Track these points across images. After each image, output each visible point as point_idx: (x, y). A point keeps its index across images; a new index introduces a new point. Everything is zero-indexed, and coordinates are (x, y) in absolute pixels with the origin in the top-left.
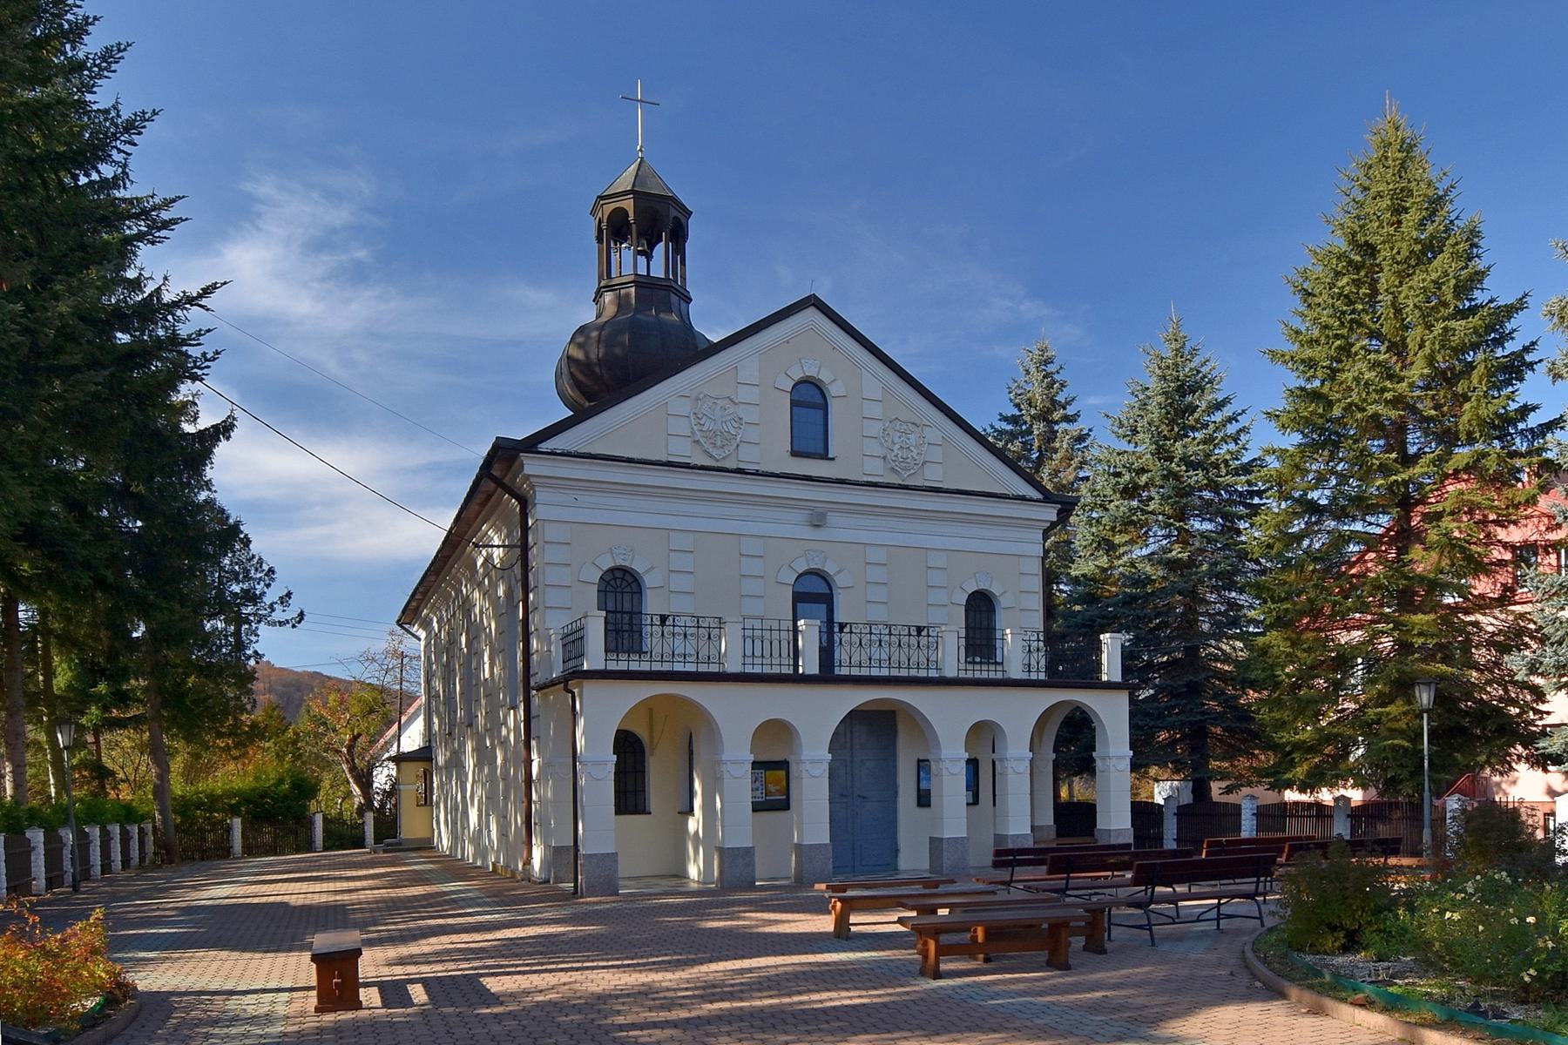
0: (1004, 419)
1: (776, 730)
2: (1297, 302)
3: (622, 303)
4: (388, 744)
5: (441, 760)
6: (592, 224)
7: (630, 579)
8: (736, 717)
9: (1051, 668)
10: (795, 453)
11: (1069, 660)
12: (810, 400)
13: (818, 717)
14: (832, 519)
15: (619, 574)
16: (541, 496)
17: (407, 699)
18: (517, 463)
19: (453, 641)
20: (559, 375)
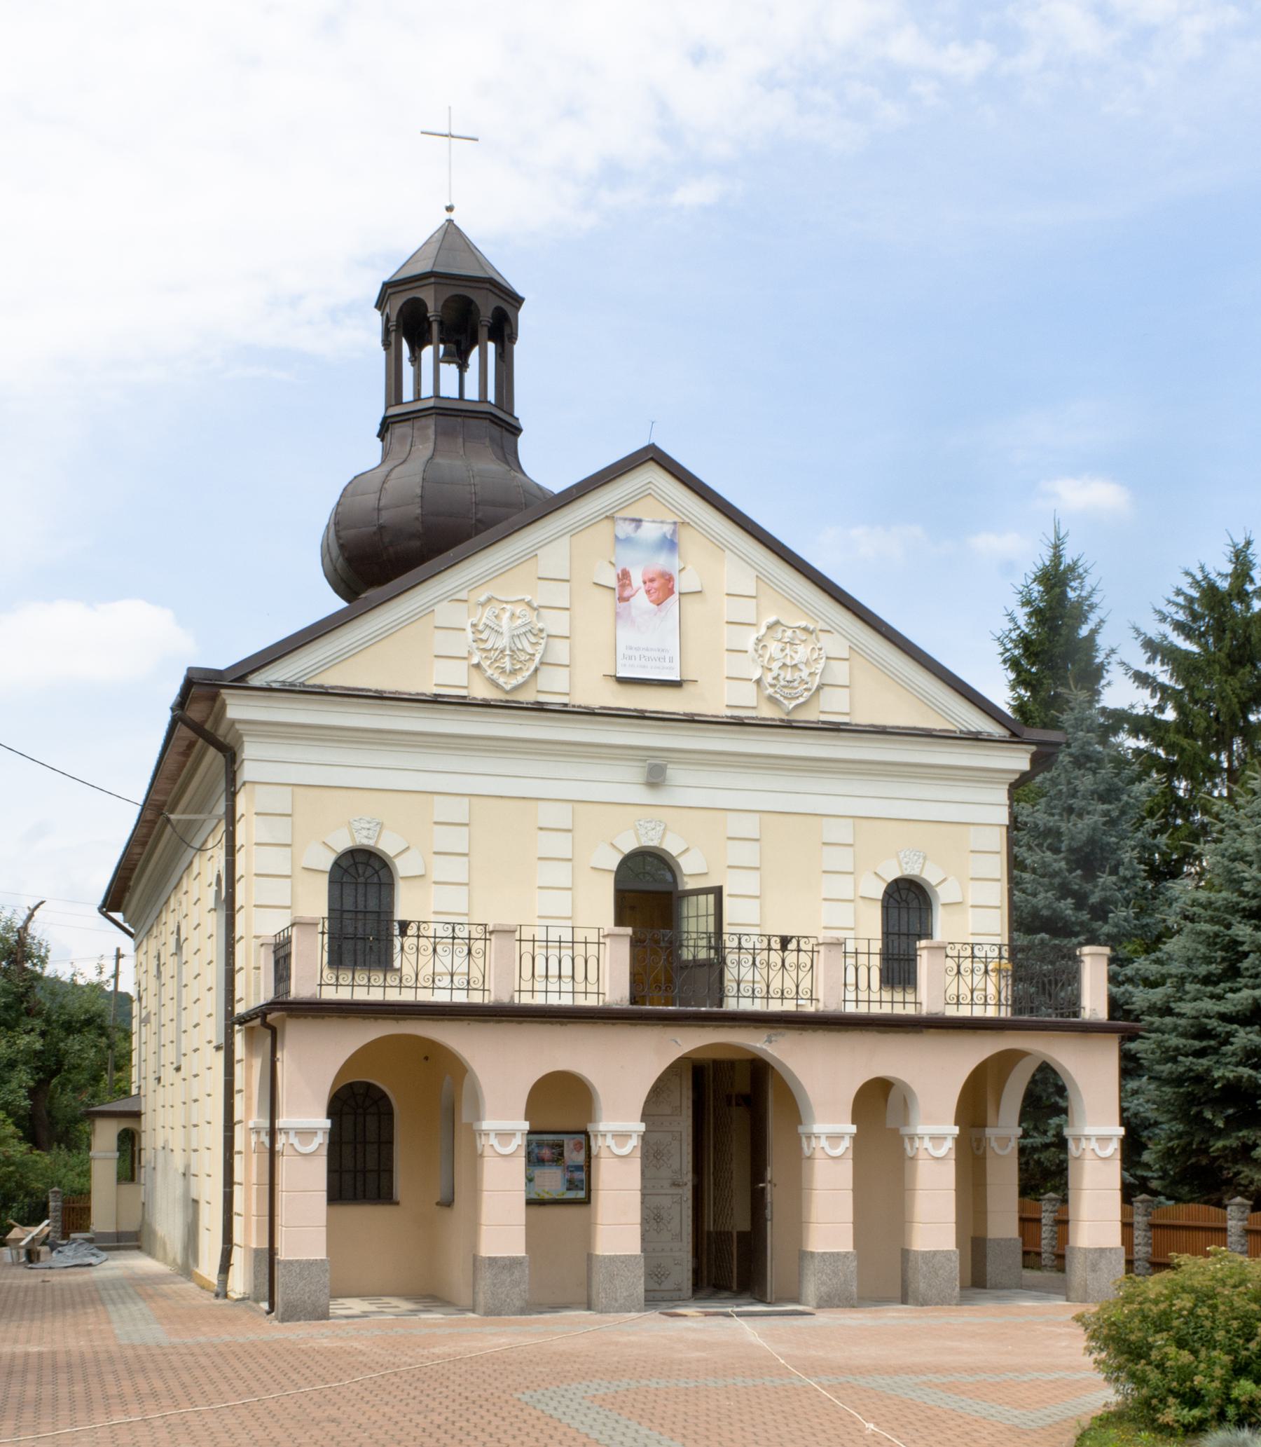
7: (377, 866)
9: (1018, 1004)
14: (676, 774)
15: (360, 859)
18: (218, 704)
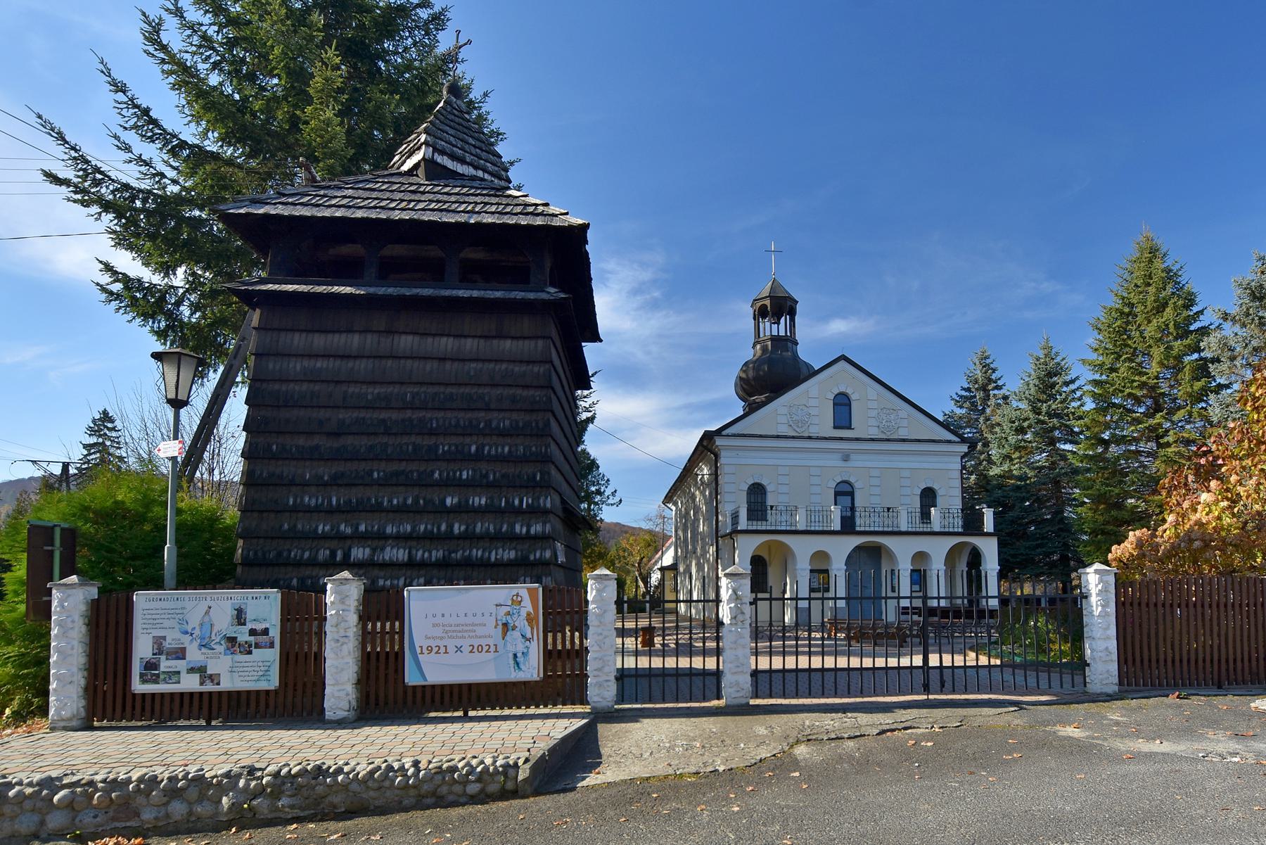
0: (963, 389)
1: (821, 556)
2: (1096, 332)
3: (764, 349)
4: (656, 562)
5: (681, 569)
6: (751, 311)
8: (803, 549)
10: (835, 427)
11: (972, 524)
12: (842, 403)
13: (840, 549)
14: (852, 456)
16: (723, 454)
17: (666, 538)
19: (687, 513)
20: (736, 385)
